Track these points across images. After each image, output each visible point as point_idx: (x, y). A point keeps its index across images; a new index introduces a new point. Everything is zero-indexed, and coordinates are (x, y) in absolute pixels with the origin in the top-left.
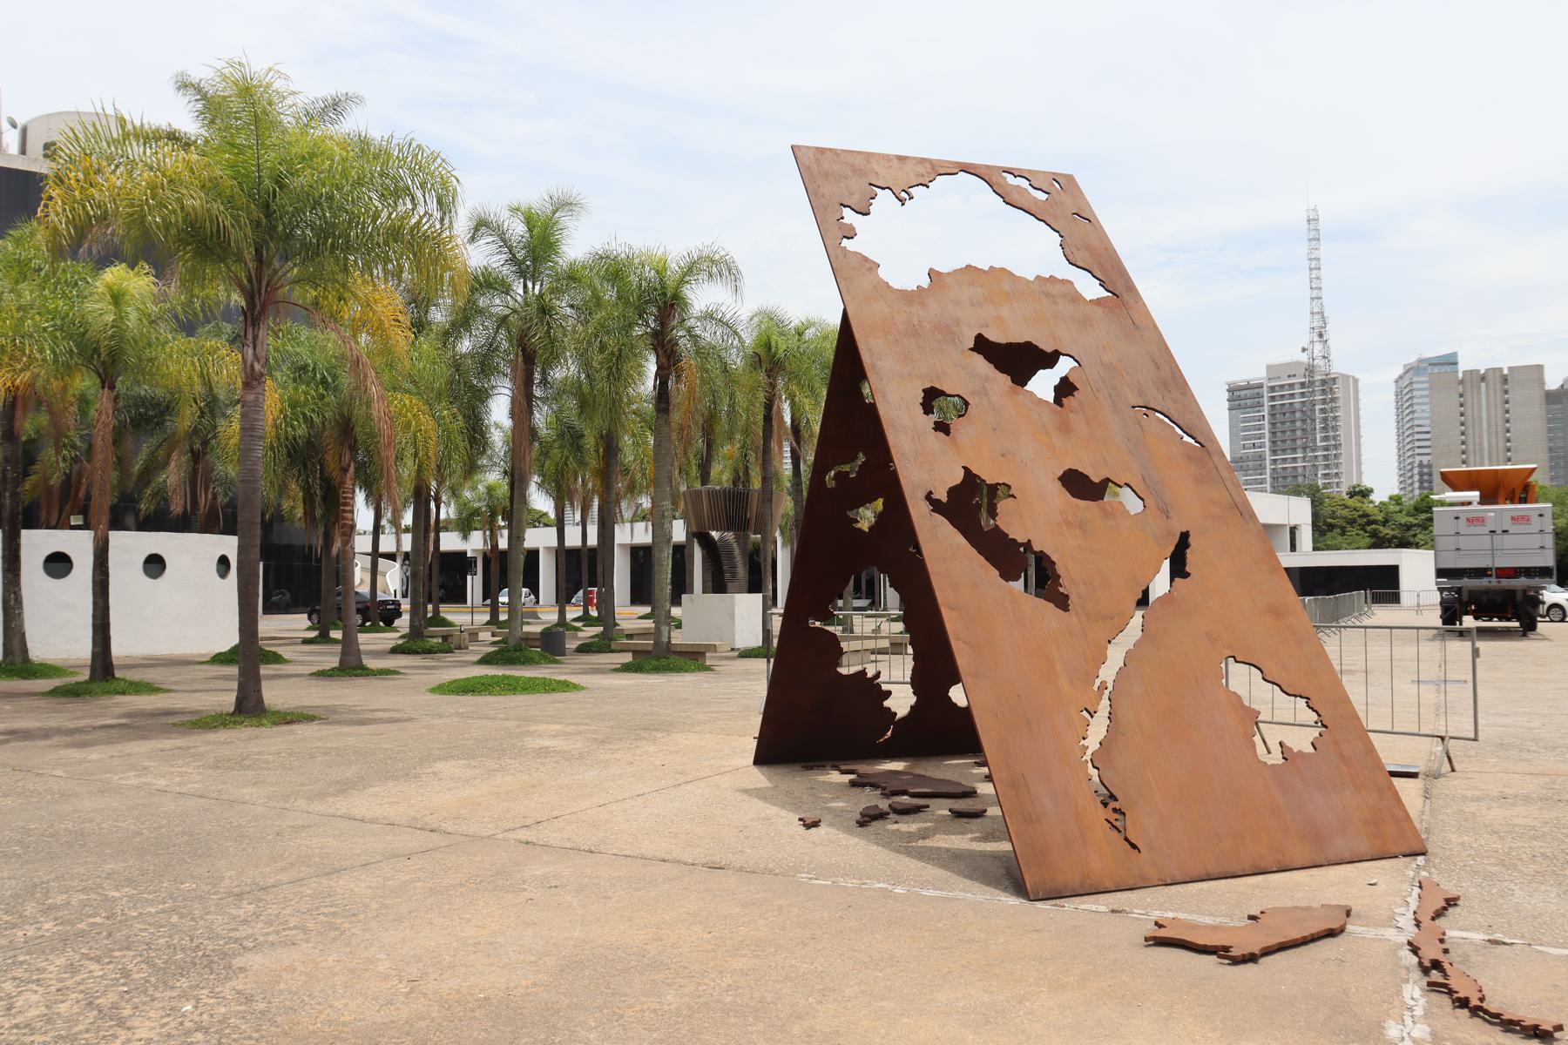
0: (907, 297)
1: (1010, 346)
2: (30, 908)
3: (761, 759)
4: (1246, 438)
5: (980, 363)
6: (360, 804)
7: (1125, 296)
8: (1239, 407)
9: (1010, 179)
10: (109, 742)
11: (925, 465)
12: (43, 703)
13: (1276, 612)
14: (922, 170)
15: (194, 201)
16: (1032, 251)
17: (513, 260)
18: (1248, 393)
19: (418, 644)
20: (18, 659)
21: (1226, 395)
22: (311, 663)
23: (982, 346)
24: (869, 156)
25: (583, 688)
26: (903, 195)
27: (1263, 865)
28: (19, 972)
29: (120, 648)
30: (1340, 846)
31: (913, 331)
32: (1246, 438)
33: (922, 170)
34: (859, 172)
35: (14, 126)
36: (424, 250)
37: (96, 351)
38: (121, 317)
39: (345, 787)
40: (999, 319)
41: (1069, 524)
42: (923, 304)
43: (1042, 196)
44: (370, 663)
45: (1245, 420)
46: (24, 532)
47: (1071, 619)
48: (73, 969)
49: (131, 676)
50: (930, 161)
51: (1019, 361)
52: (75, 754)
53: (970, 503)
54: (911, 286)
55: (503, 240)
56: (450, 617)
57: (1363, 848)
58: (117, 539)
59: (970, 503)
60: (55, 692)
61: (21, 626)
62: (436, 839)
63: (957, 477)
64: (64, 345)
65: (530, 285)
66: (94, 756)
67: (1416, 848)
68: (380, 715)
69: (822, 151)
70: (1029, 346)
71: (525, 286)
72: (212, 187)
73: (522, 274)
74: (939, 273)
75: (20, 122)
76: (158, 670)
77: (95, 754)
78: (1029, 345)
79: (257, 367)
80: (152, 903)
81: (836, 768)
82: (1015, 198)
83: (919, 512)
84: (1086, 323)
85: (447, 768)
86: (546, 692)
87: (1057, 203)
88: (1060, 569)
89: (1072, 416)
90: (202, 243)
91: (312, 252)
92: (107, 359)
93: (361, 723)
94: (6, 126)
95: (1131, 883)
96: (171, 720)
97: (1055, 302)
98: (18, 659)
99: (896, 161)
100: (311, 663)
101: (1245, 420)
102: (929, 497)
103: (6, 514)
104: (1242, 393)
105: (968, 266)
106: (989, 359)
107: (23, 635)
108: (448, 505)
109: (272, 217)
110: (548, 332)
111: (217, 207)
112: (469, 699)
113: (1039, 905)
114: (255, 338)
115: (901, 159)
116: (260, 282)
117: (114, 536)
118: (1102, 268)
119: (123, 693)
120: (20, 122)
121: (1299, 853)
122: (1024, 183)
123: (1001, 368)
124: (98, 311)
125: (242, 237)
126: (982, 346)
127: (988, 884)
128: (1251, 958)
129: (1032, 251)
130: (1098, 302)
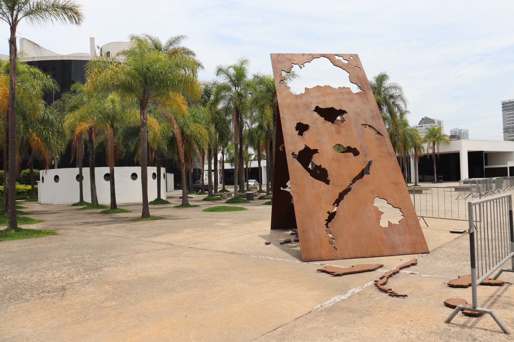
0: (297, 97)
1: (326, 109)
2: (67, 258)
3: (272, 228)
4: (509, 121)
5: (316, 115)
6: (158, 239)
7: (367, 91)
8: (506, 110)
9: (337, 58)
10: (107, 224)
11: (293, 143)
12: (99, 215)
13: (396, 184)
14: (309, 57)
15: (122, 77)
16: (340, 79)
17: (231, 81)
18: (510, 104)
19: (211, 198)
20: (95, 204)
21: (501, 106)
22: (175, 204)
23: (318, 110)
24: (293, 55)
25: (247, 209)
26: (302, 66)
27: (375, 255)
28: (58, 269)
29: (119, 201)
30: (401, 250)
31: (297, 107)
32: (509, 121)
33: (309, 57)
34: (289, 60)
35: (99, 48)
36: (187, 85)
37: (109, 117)
38: (114, 107)
39: (156, 235)
40: (324, 101)
41: (334, 160)
42: (301, 98)
43: (346, 62)
44: (191, 203)
45: (509, 114)
46: (148, 168)
47: (329, 187)
48: (69, 269)
49: (121, 208)
50: (312, 55)
51: (330, 114)
52: (97, 227)
53: (306, 156)
54: (298, 93)
55: (228, 75)
56: (228, 189)
57: (408, 251)
58: (97, 170)
59: (306, 156)
60: (101, 213)
61: (96, 194)
62: (170, 246)
63: (302, 148)
64: (100, 116)
65: (237, 88)
66: (101, 228)
67: (426, 251)
68: (182, 217)
69: (279, 54)
70: (332, 109)
71: (236, 89)
72: (128, 74)
73: (235, 85)
74: (308, 89)
75: (100, 47)
76: (133, 207)
77: (101, 227)
78: (332, 108)
79: (144, 121)
80: (92, 258)
81: (291, 230)
82: (337, 63)
83: (289, 158)
84: (352, 100)
85: (187, 230)
86: (235, 211)
87: (352, 65)
88: (329, 173)
89: (341, 129)
90: (125, 88)
91: (158, 88)
92: (111, 118)
93: (175, 219)
94: (96, 48)
95: (333, 258)
96: (125, 219)
97: (343, 95)
98: (95, 204)
99: (301, 56)
100: (175, 204)
101: (509, 114)
102: (293, 154)
103: (90, 163)
104: (507, 105)
105: (318, 86)
106: (318, 113)
107: (96, 197)
108: (226, 154)
109: (154, 75)
110: (241, 101)
111: (129, 78)
112: (212, 213)
113: (304, 263)
114: (144, 113)
115: (303, 55)
116: (144, 97)
117: (116, 168)
118: (361, 83)
119: (118, 213)
120: (100, 47)
121: (386, 252)
122: (341, 58)
123: (321, 116)
124: (108, 105)
125: (137, 84)
126: (318, 110)
127: (294, 257)
128: (339, 275)
129: (340, 79)
130: (357, 94)
